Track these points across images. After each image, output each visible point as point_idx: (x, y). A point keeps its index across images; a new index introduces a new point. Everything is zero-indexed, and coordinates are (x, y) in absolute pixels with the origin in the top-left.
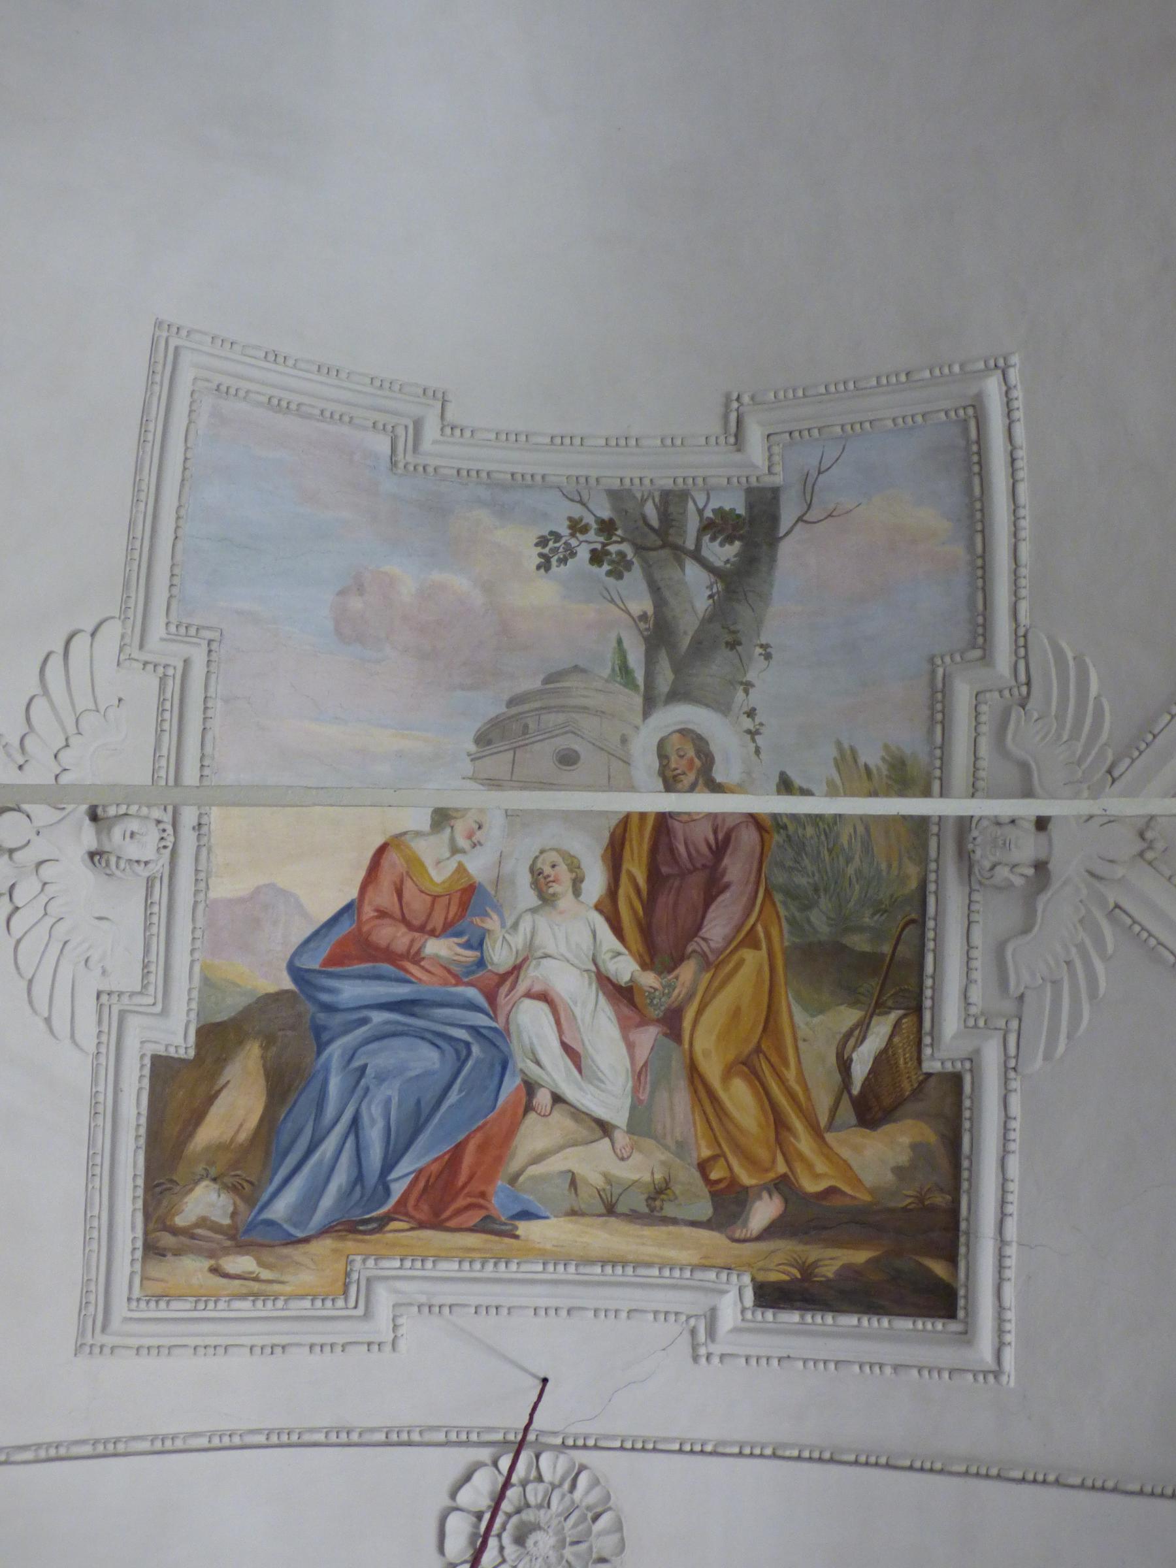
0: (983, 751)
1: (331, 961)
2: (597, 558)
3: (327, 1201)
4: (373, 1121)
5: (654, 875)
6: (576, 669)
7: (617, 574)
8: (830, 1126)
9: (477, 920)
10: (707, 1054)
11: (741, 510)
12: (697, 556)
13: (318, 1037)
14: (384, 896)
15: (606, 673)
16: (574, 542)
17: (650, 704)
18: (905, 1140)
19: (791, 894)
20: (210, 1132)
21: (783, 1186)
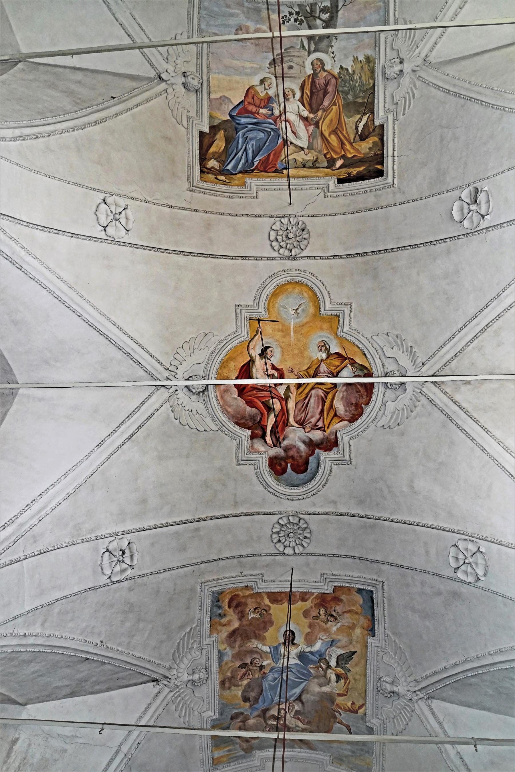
0: (387, 50)
1: (238, 113)
2: (296, 20)
3: (240, 166)
4: (250, 149)
5: (312, 92)
6: (292, 47)
7: (300, 24)
8: (354, 142)
9: (271, 105)
10: (325, 130)
11: (329, 6)
12: (319, 18)
13: (236, 130)
14: (250, 100)
15: (299, 47)
16: (290, 17)
17: (309, 53)
18: (371, 142)
19: (342, 92)
20: (212, 149)
21: (343, 157)
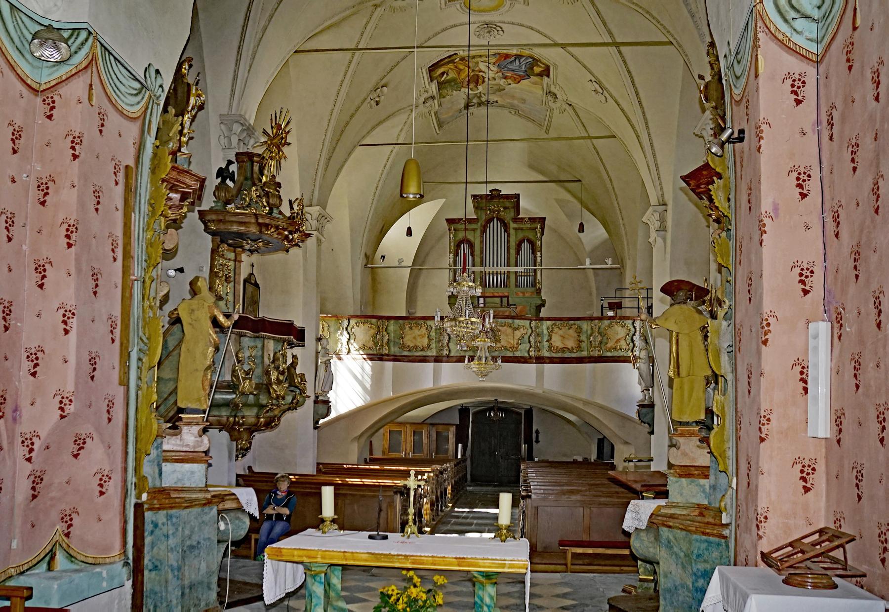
17: (480, 93)
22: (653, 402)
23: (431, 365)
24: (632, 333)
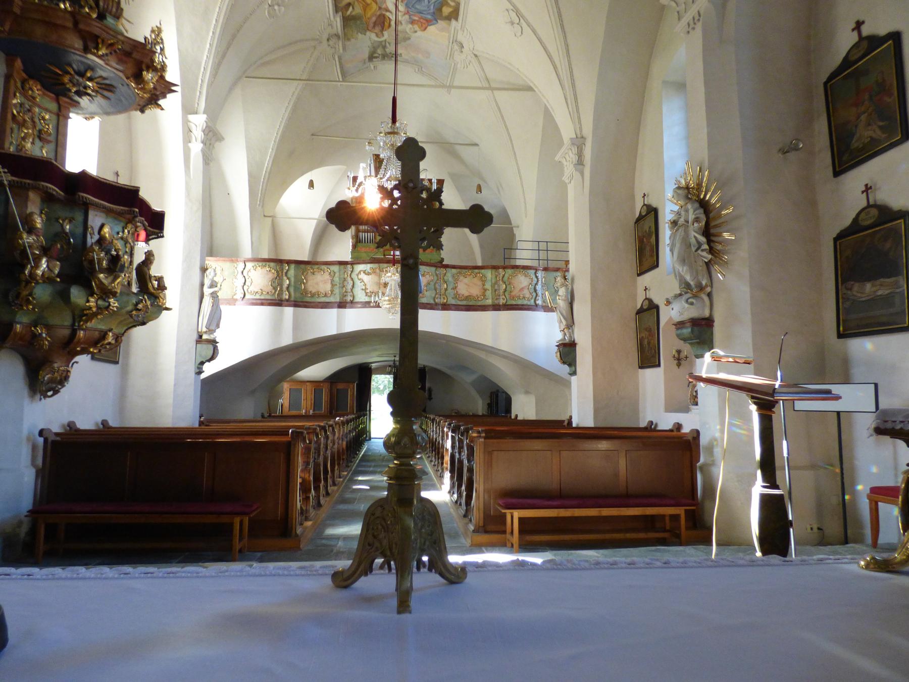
12: (379, 55)
17: (385, 41)
22: (574, 341)
23: (334, 311)
24: (535, 282)
